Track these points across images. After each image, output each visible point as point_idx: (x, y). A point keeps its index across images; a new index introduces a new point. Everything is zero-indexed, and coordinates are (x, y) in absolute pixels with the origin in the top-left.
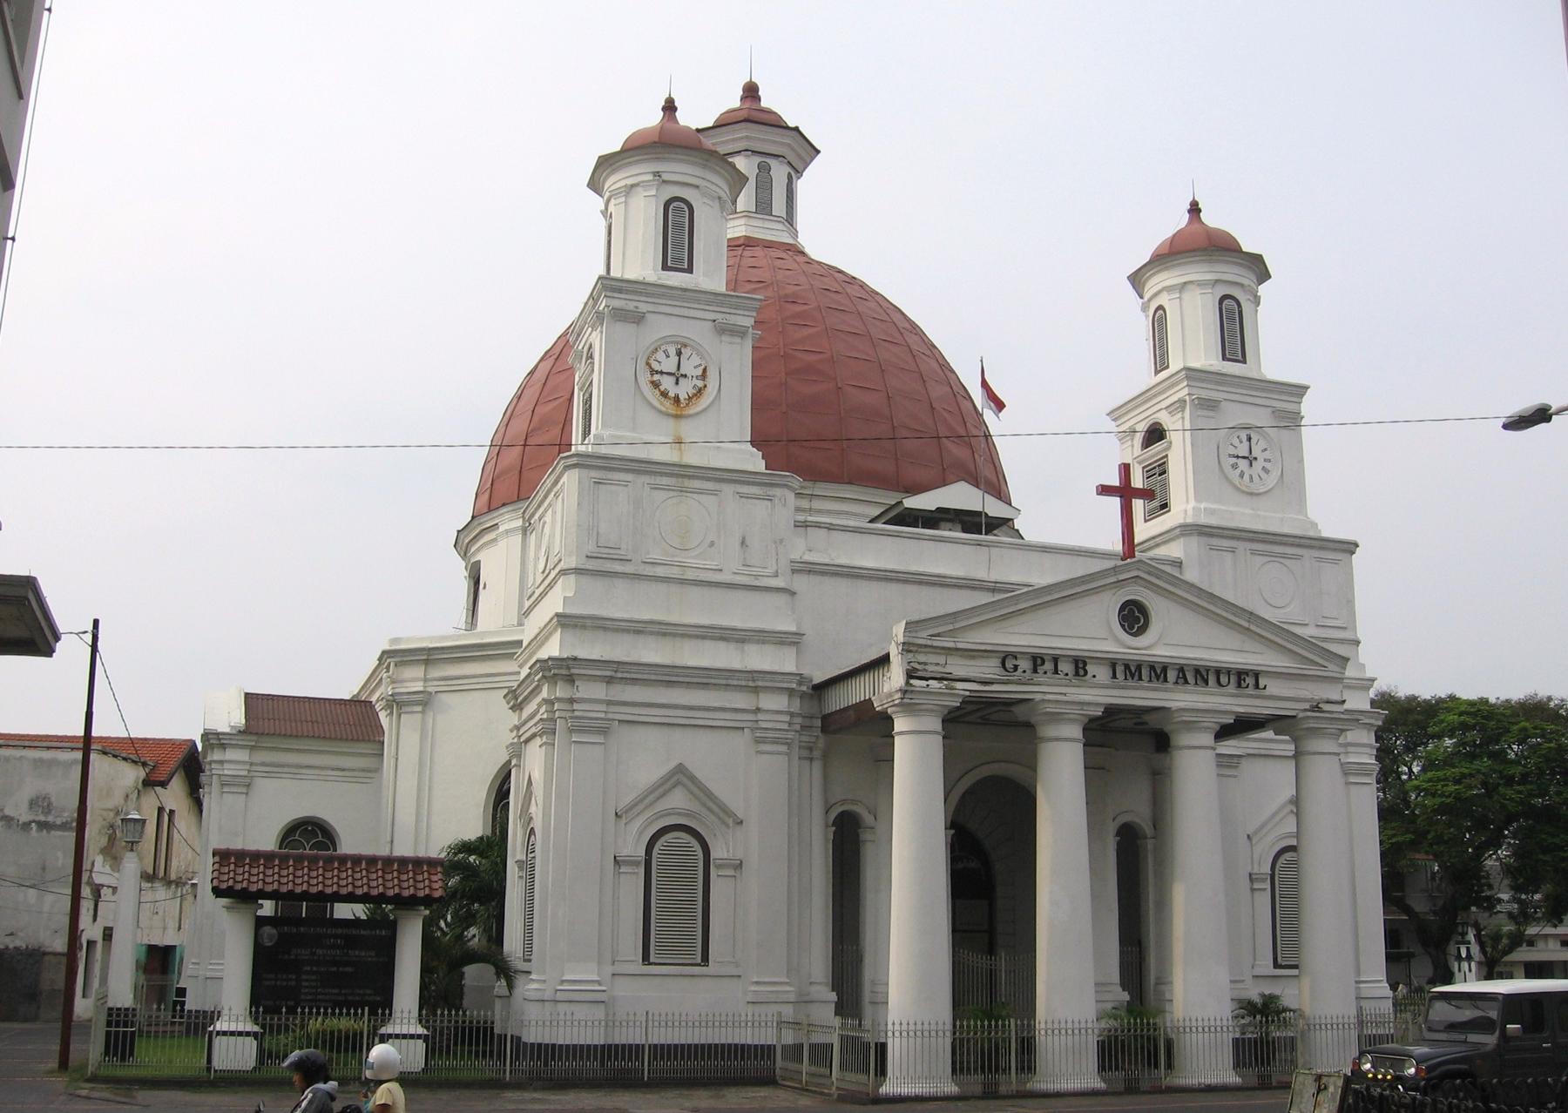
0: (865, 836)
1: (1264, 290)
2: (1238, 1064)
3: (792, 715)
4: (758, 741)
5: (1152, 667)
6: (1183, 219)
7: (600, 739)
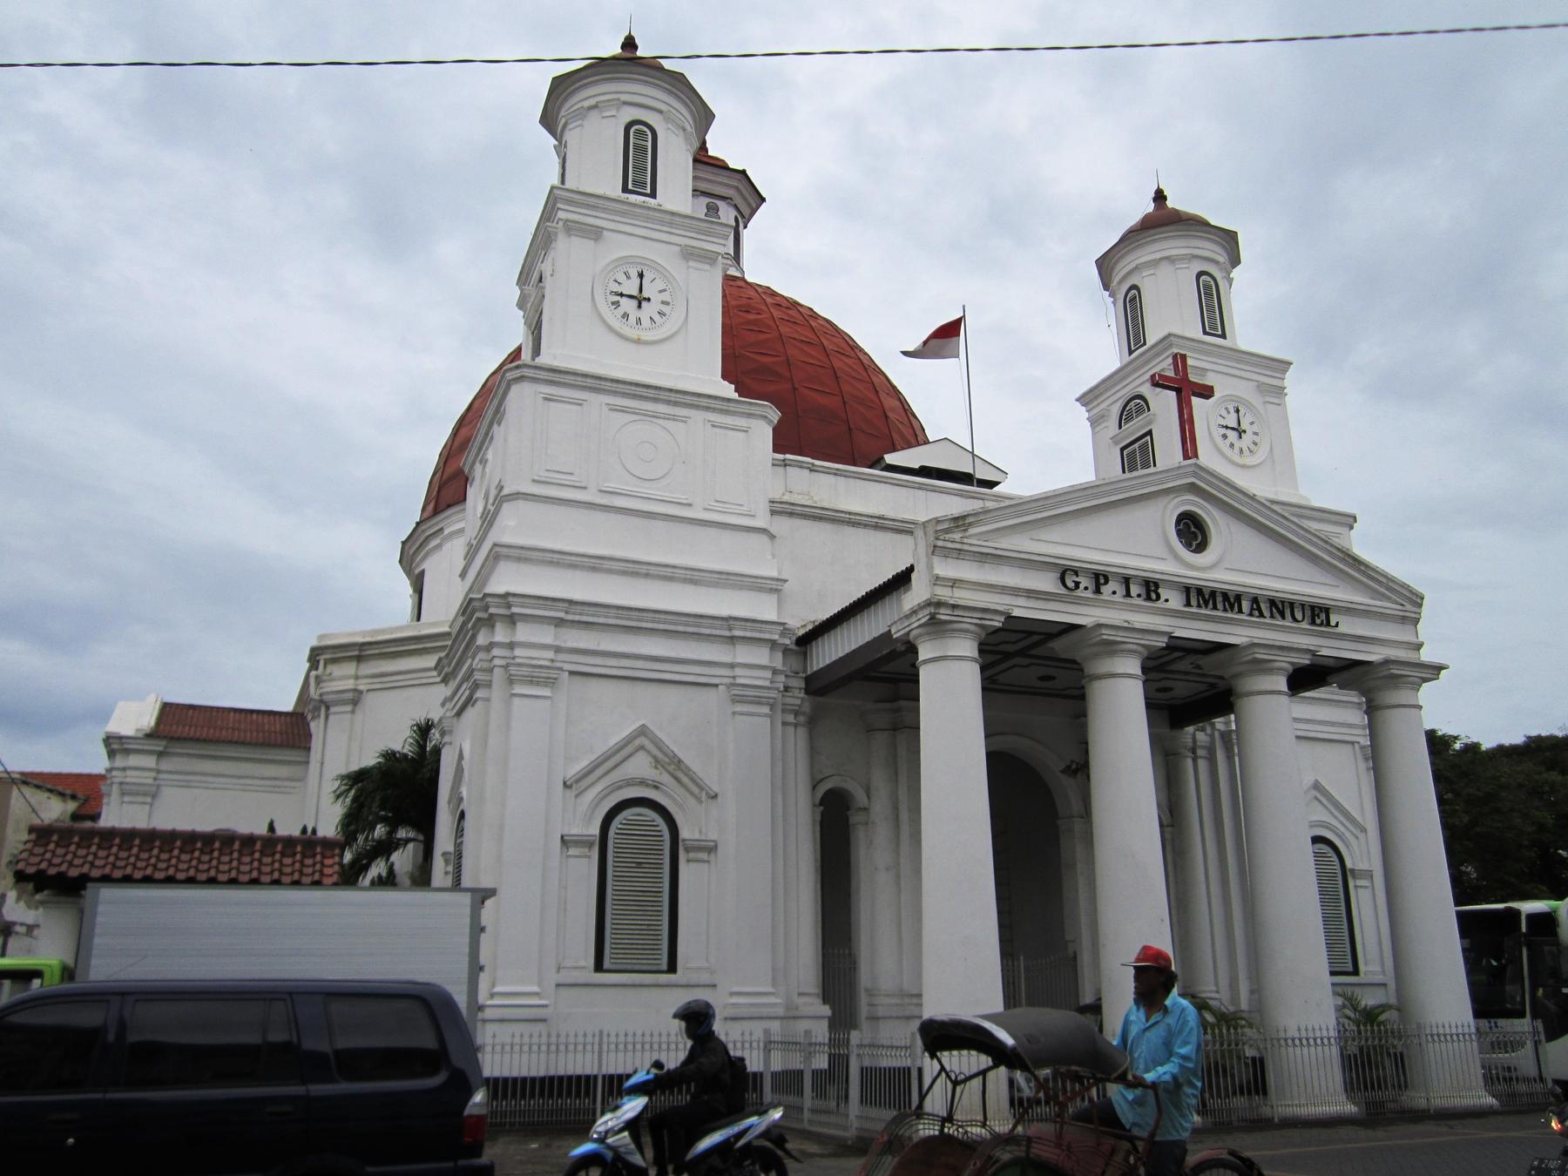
0: (855, 818)
1: (1235, 273)
2: (1350, 1088)
3: (775, 672)
4: (737, 700)
5: (1225, 595)
6: (1151, 207)
7: (546, 692)
